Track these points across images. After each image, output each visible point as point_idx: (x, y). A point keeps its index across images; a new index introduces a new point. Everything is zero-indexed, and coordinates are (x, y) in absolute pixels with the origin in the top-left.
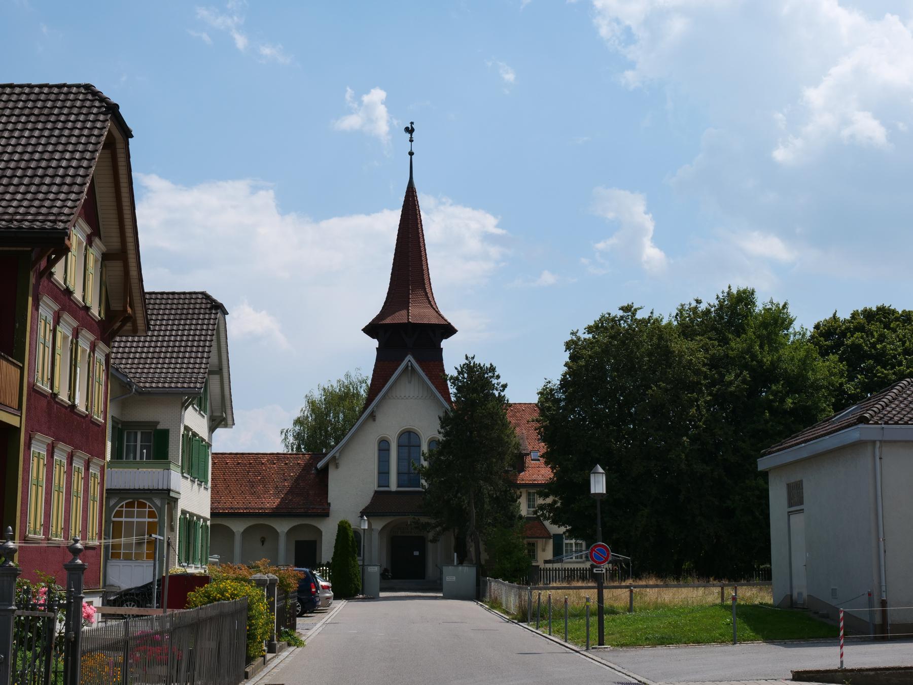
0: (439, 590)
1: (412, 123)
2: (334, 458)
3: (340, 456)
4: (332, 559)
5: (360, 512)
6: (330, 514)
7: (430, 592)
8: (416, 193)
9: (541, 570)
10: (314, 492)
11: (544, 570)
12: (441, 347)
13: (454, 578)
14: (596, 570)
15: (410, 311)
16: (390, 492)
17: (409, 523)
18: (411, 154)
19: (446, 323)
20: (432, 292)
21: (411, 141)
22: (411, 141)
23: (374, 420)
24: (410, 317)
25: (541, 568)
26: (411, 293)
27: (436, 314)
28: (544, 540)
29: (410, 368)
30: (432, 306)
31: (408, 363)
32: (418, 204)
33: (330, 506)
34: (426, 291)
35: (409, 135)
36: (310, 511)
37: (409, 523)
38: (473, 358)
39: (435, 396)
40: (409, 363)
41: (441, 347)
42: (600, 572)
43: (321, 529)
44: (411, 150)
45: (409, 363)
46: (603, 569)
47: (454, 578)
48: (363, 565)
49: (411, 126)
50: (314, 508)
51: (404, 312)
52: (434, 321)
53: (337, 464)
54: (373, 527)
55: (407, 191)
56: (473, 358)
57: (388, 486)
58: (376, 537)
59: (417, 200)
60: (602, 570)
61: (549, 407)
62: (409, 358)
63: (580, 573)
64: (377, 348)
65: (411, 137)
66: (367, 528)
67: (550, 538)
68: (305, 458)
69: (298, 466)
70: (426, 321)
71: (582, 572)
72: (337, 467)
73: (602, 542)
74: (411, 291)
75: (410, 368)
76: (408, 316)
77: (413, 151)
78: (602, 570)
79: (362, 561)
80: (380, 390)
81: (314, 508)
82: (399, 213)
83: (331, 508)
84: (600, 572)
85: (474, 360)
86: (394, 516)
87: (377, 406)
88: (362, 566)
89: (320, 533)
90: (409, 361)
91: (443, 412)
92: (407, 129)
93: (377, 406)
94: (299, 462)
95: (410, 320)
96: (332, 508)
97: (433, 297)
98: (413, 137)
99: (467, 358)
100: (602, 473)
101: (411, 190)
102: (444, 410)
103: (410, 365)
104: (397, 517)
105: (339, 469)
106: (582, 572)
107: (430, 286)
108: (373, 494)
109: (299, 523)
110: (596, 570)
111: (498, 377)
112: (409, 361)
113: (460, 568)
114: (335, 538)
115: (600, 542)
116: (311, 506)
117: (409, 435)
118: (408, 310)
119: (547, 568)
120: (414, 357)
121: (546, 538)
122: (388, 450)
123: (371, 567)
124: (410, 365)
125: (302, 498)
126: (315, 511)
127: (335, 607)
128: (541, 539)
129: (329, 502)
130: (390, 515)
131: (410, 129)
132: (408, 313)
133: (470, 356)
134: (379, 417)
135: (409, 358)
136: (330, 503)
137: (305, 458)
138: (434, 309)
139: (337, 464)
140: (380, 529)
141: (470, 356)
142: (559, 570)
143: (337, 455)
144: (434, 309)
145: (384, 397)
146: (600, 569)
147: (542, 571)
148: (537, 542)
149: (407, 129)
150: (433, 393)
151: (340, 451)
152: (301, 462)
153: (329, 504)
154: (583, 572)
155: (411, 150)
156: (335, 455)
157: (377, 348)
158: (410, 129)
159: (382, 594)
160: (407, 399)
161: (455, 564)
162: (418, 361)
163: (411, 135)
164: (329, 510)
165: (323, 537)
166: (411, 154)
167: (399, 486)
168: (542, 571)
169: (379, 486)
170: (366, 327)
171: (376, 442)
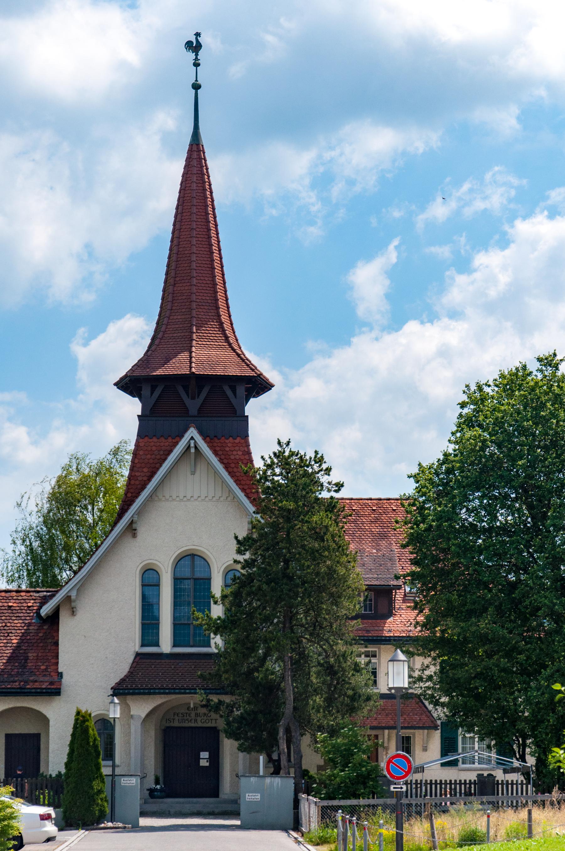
0: (235, 814)
1: (198, 35)
2: (68, 599)
3: (77, 595)
4: (67, 765)
5: (112, 688)
6: (62, 690)
7: (232, 819)
8: (204, 153)
9: (498, 784)
10: (35, 655)
11: (502, 784)
12: (246, 414)
13: (258, 797)
14: (394, 788)
15: (194, 354)
16: (160, 656)
17: (192, 706)
18: (196, 87)
19: (253, 374)
20: (231, 321)
21: (196, 65)
22: (196, 65)
23: (134, 536)
24: (193, 365)
25: (498, 781)
26: (195, 331)
27: (238, 360)
28: (426, 731)
29: (193, 450)
30: (230, 345)
31: (189, 441)
32: (207, 172)
33: (62, 677)
34: (220, 320)
35: (193, 56)
36: (28, 687)
37: (192, 706)
38: (288, 443)
39: (235, 497)
40: (192, 442)
41: (246, 414)
42: (399, 790)
43: (48, 716)
44: (196, 80)
45: (192, 442)
46: (402, 786)
47: (258, 797)
48: (113, 775)
49: (197, 41)
50: (36, 681)
51: (184, 356)
52: (234, 371)
53: (73, 608)
54: (132, 713)
55: (185, 166)
56: (288, 443)
57: (157, 644)
58: (136, 727)
59: (206, 165)
60: (401, 788)
61: (221, 661)
62: (192, 432)
63: (451, 789)
64: (138, 416)
65: (196, 59)
66: (118, 716)
67: (435, 728)
68: (20, 598)
69: (10, 611)
70: (220, 372)
71: (453, 786)
72: (73, 612)
73: (403, 751)
74: (194, 328)
75: (193, 450)
76: (191, 362)
77: (200, 81)
78: (401, 788)
79: (111, 769)
80: (143, 487)
81: (36, 681)
82: (183, 163)
83: (63, 680)
84: (399, 790)
85: (290, 447)
86: (167, 694)
87: (139, 512)
88: (111, 778)
89: (45, 721)
90: (192, 438)
91: (248, 523)
92: (189, 45)
93: (139, 512)
94: (10, 604)
95: (193, 370)
96: (66, 680)
97: (233, 330)
98: (199, 57)
99: (279, 443)
100: (404, 661)
101: (195, 163)
102: (250, 520)
103: (192, 445)
104: (173, 697)
105: (75, 617)
106: (453, 786)
107: (228, 311)
108: (132, 658)
109: (11, 706)
110: (394, 788)
111: (328, 471)
112: (192, 438)
113: (268, 780)
114: (71, 731)
115: (400, 750)
116: (32, 678)
117: (193, 561)
118: (191, 352)
119: (507, 781)
120: (201, 433)
121: (429, 728)
122: (157, 585)
123: (125, 779)
124: (192, 445)
125: (17, 664)
126: (37, 685)
127: (66, 841)
128: (421, 731)
129: (60, 670)
130: (160, 693)
131: (194, 45)
132: (191, 357)
133: (284, 441)
134: (142, 530)
135: (192, 432)
136: (61, 673)
137: (20, 598)
138: (234, 350)
139: (73, 608)
140: (143, 715)
141: (284, 441)
142: (512, 784)
143: (73, 594)
144: (234, 350)
145: (151, 497)
146: (399, 786)
147: (500, 786)
148: (414, 734)
149: (189, 45)
150: (230, 491)
151: (77, 588)
152: (15, 605)
153: (60, 675)
154: (416, 786)
155: (196, 80)
156: (69, 594)
157: (138, 416)
158: (194, 45)
159: (144, 822)
160: (188, 500)
161: (261, 773)
162: (205, 436)
163: (197, 55)
164: (61, 685)
165: (50, 728)
166: (196, 87)
167: (175, 645)
168: (500, 786)
169: (143, 645)
170: (122, 379)
171: (138, 572)
